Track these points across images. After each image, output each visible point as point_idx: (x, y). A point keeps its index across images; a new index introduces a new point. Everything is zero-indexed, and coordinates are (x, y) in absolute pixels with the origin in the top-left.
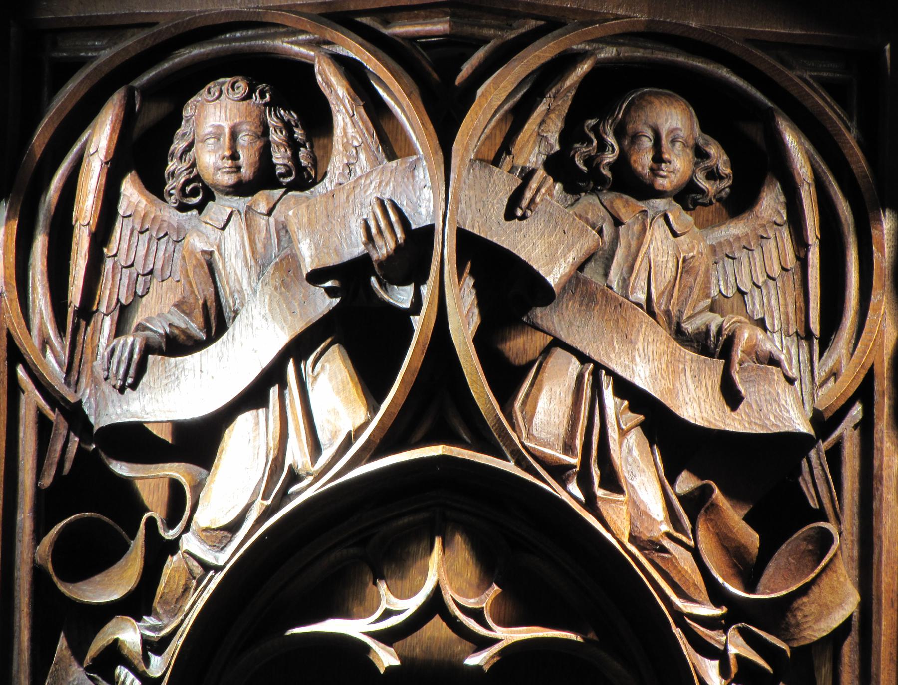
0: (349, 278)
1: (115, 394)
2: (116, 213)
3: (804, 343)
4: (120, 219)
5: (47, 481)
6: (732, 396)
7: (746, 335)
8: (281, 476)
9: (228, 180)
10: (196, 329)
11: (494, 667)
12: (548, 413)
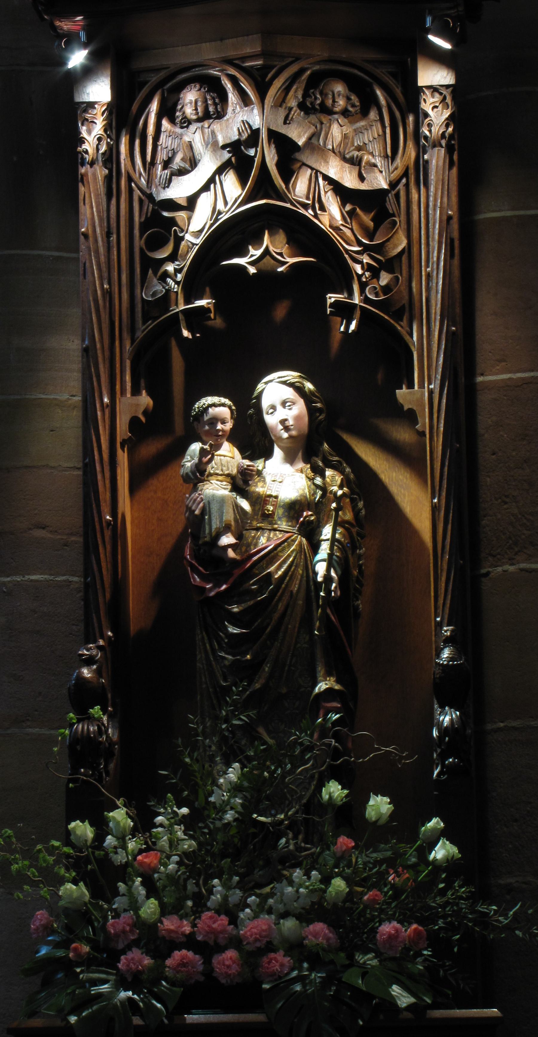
0: (234, 147)
1: (162, 190)
2: (161, 131)
3: (386, 159)
4: (162, 133)
5: (143, 219)
6: (362, 178)
7: (365, 158)
8: (216, 214)
9: (194, 117)
10: (187, 166)
11: (287, 271)
12: (301, 187)
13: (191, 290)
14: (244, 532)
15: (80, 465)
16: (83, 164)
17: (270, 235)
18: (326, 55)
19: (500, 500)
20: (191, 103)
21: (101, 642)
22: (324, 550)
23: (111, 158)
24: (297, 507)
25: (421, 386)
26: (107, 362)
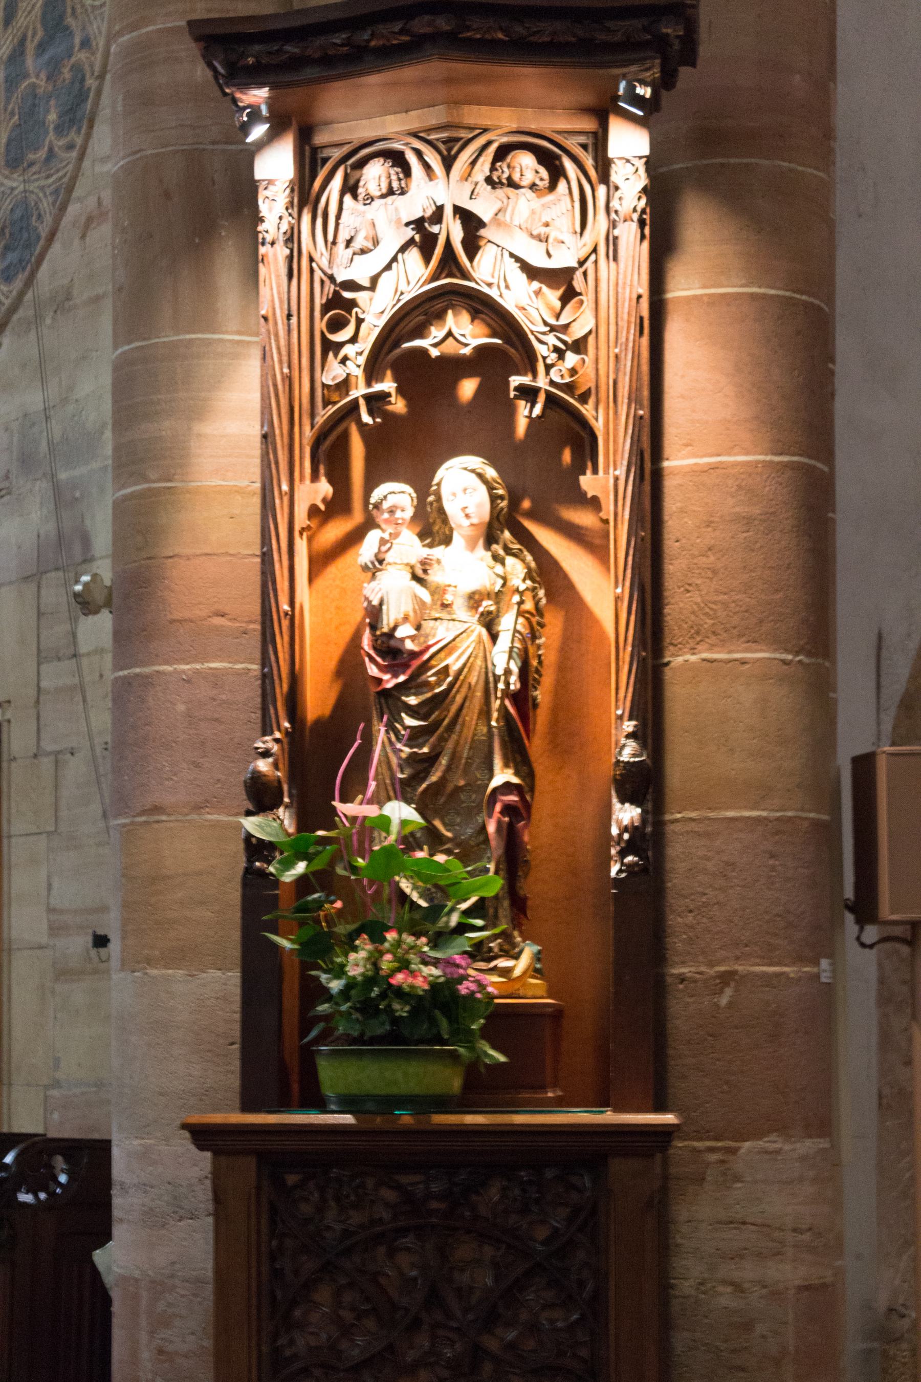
0: (418, 224)
5: (324, 301)
9: (379, 194)
10: (370, 246)
13: (372, 372)
14: (423, 622)
15: (258, 553)
16: (263, 244)
17: (455, 315)
18: (514, 126)
19: (682, 589)
20: (374, 179)
21: (278, 735)
22: (505, 641)
23: (292, 237)
24: (477, 597)
25: (606, 472)
26: (286, 448)
